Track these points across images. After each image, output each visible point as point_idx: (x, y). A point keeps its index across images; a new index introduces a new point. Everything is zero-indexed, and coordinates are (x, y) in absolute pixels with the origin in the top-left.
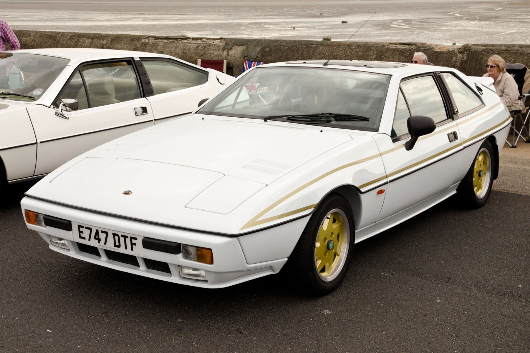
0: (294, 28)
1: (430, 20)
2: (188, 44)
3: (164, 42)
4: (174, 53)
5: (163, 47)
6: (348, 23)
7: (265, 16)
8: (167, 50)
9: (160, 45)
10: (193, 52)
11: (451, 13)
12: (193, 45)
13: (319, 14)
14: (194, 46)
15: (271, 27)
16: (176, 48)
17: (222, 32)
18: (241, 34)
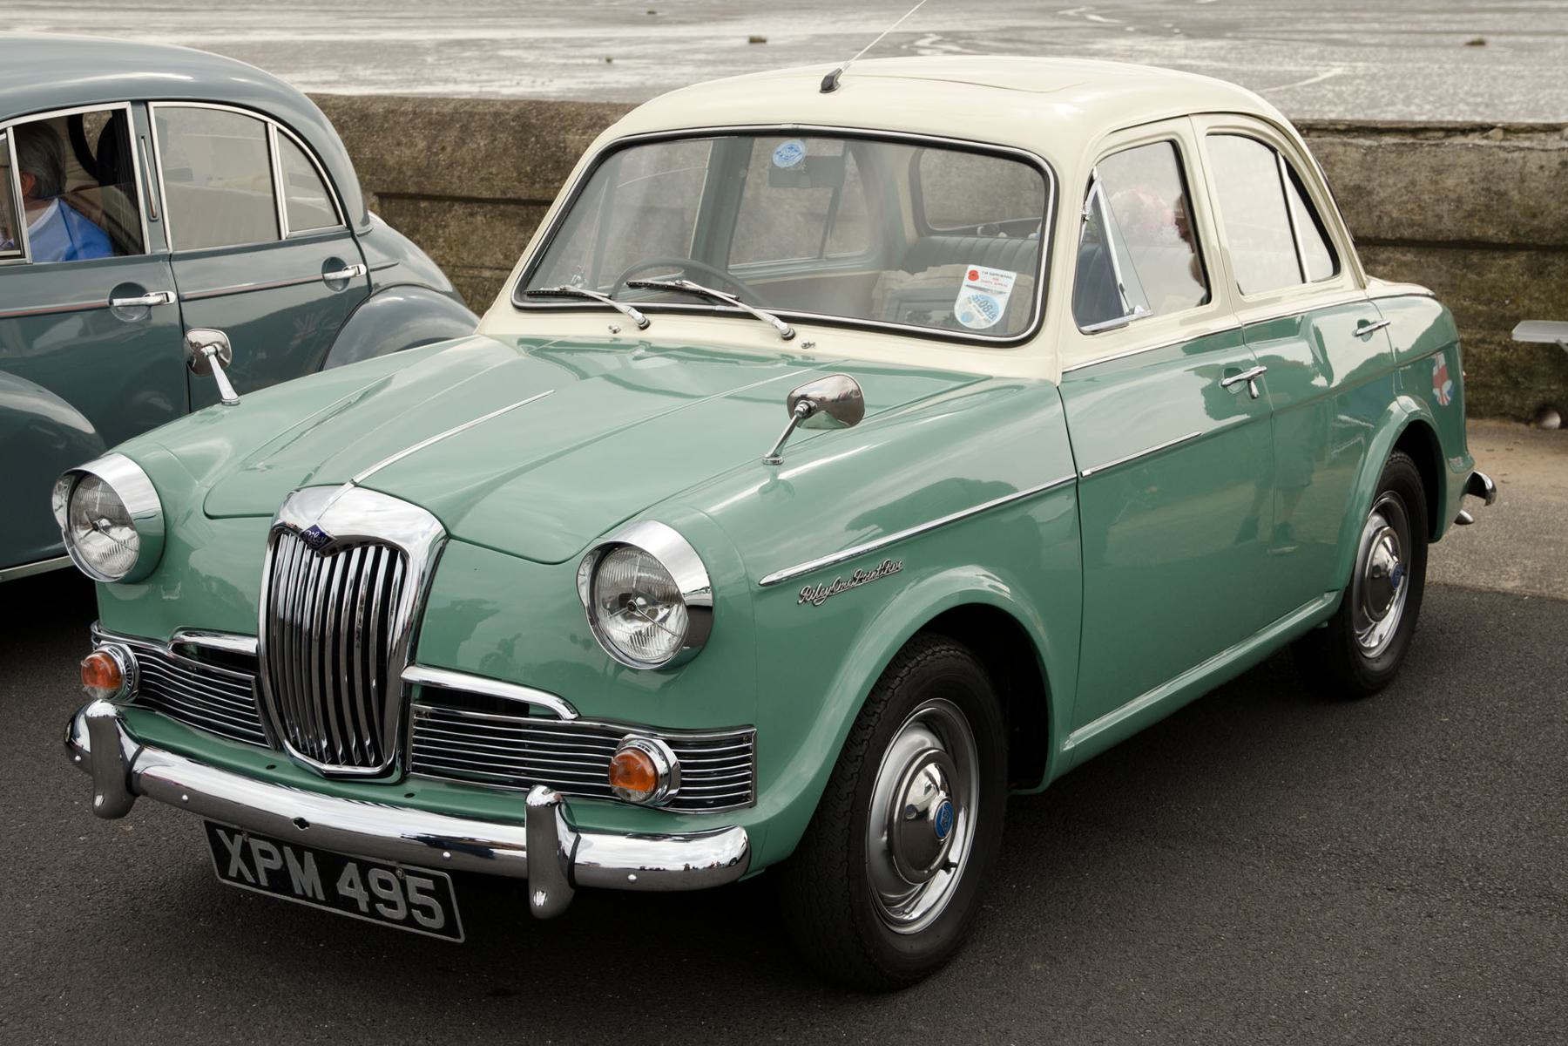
0: (609, 60)
1: (1028, 36)
2: (1502, 154)
3: (1358, 147)
4: (1430, 192)
5: (1361, 167)
6: (769, 43)
7: (463, 17)
8: (1391, 181)
9: (1341, 160)
10: (1542, 188)
11: (1071, 13)
12: (1534, 160)
13: (645, 14)
14: (1544, 163)
15: (530, 56)
16: (1438, 171)
17: (373, 74)
18: (446, 81)
